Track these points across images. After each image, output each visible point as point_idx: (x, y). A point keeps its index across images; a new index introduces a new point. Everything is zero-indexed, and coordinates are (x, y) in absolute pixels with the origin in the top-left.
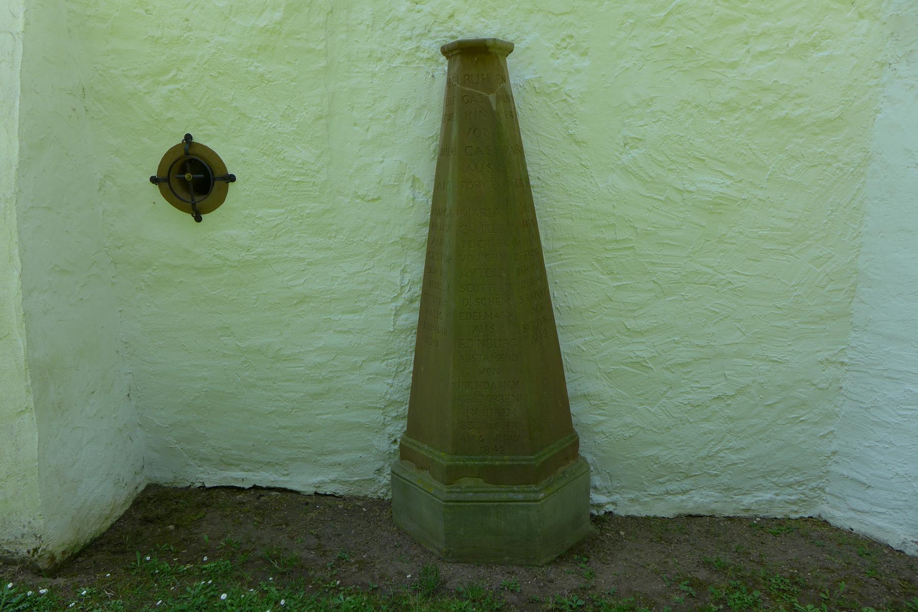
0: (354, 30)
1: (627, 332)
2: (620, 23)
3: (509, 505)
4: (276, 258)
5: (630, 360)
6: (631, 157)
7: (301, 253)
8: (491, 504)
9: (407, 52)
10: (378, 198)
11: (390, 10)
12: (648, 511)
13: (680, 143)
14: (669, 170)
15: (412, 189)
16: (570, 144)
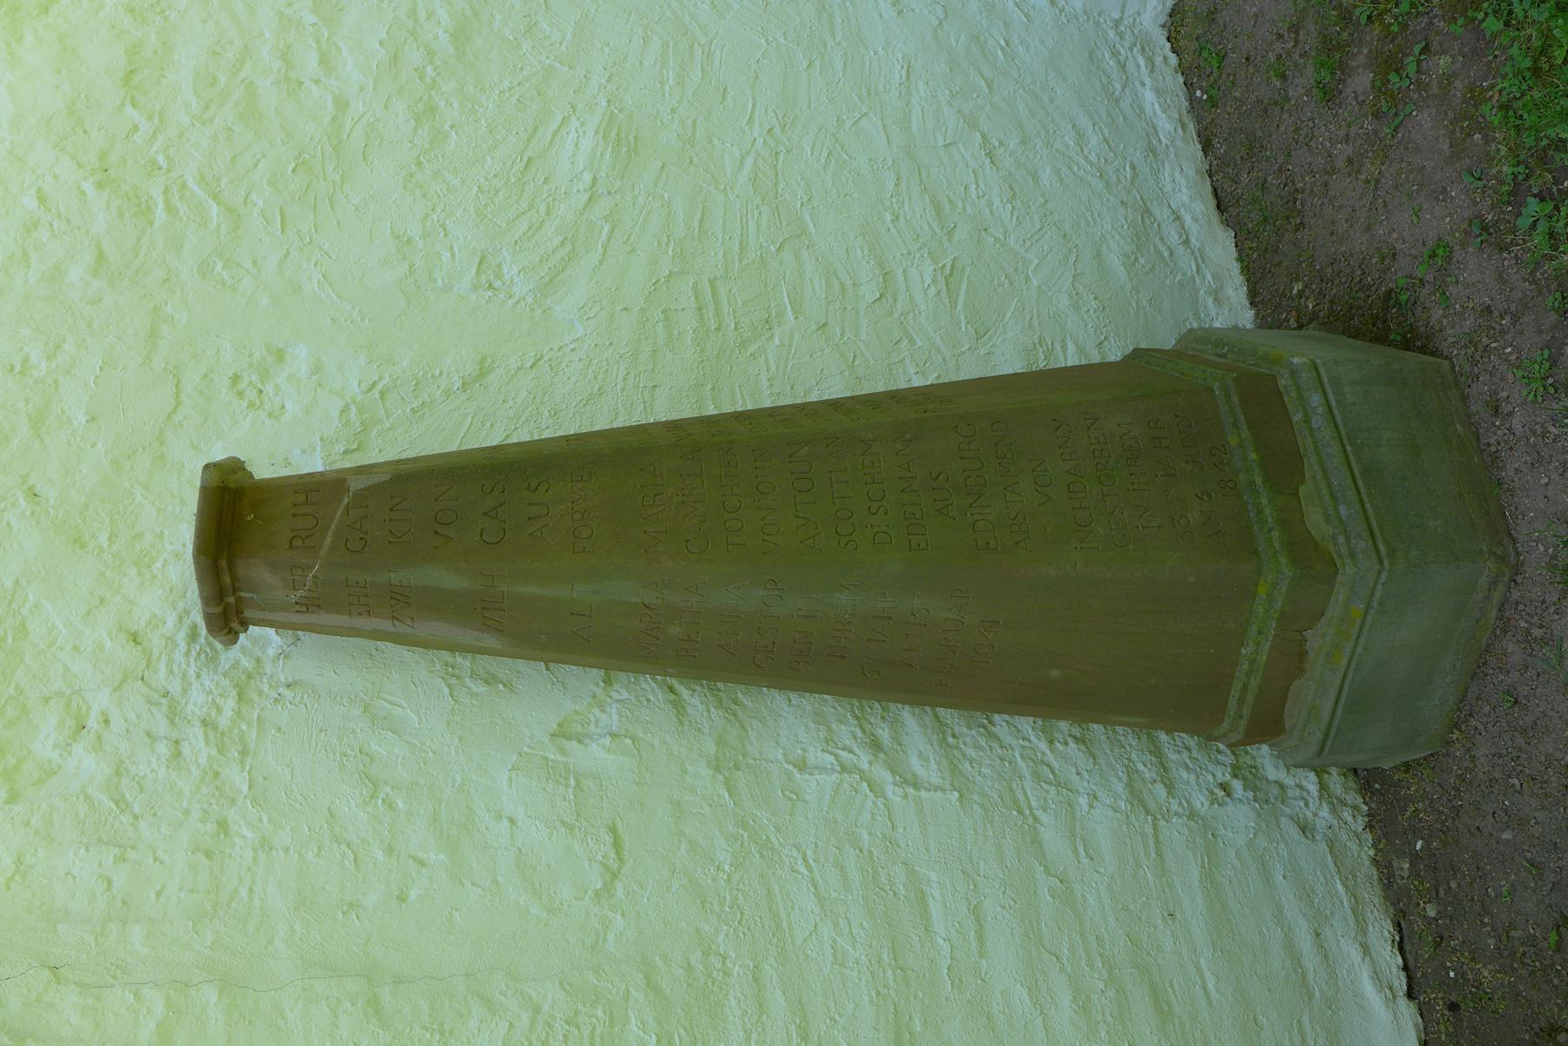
0: (124, 902)
2: (219, 287)
5: (944, 295)
6: (518, 276)
9: (214, 752)
10: (613, 830)
11: (87, 797)
14: (548, 213)
16: (485, 388)
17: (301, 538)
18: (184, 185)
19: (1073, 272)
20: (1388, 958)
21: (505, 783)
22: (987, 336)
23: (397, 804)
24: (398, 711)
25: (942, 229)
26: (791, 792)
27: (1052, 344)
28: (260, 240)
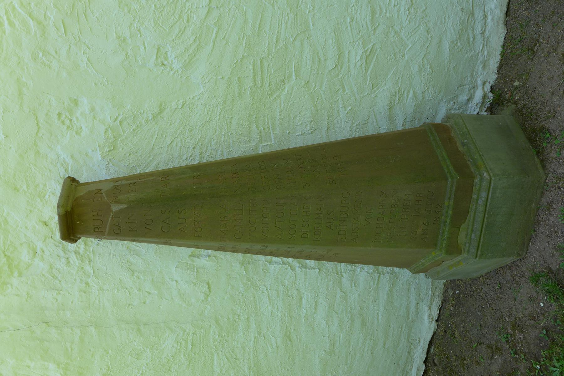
0: (62, 305)
1: (338, 68)
2: (43, 66)
3: (489, 205)
4: (254, 357)
5: (363, 66)
6: (175, 59)
7: (250, 340)
8: (485, 220)
9: (80, 262)
10: (208, 284)
11: (43, 275)
12: (496, 53)
13: (162, 9)
14: (188, 22)
15: (200, 257)
16: (162, 118)
17: (98, 228)
18: (14, 8)
19: (425, 52)
20: (435, 311)
21: (174, 271)
22: (377, 87)
23: (140, 277)
24: (139, 248)
25: (372, 27)
26: (265, 270)
27: (404, 92)
28: (56, 39)
